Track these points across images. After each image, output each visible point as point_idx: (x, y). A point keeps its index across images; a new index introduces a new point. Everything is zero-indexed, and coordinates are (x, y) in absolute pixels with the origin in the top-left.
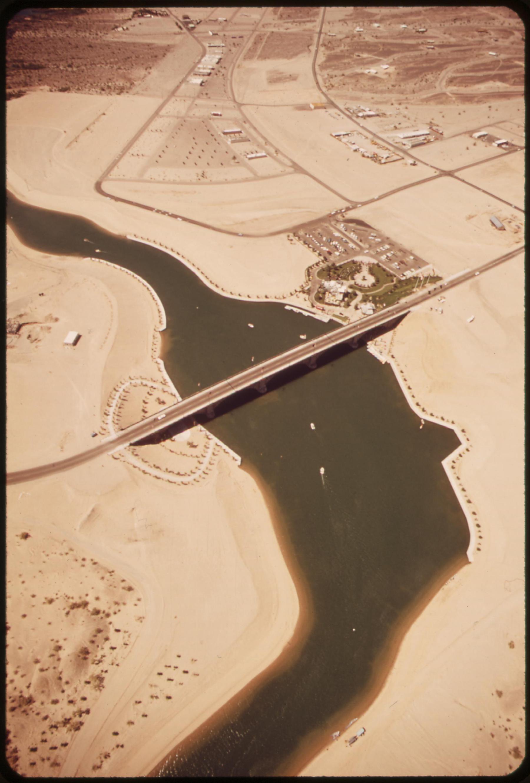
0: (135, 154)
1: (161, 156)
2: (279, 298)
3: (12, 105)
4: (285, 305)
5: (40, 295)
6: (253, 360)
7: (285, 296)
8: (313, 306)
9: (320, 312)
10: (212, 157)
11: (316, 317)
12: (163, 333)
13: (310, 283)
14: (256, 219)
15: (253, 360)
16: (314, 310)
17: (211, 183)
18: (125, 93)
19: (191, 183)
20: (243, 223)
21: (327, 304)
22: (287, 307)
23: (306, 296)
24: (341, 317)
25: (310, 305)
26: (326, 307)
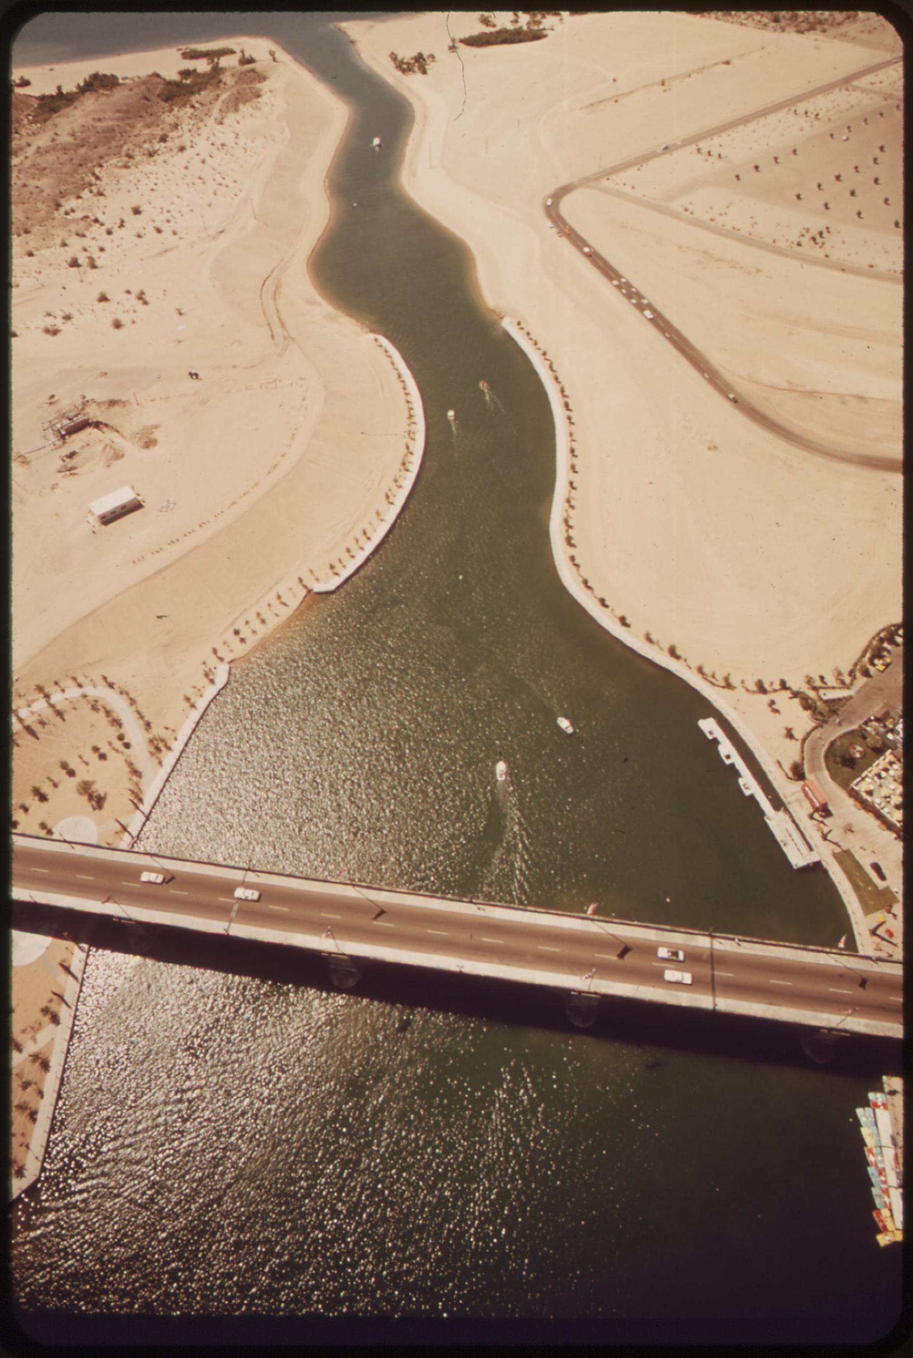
0: (714, 159)
1: (760, 169)
2: (710, 679)
3: (897, 617)
4: (711, 711)
5: (191, 375)
6: (515, 1236)
7: (734, 680)
8: (798, 773)
9: (801, 811)
10: (886, 201)
11: (776, 822)
12: (315, 598)
13: (861, 680)
14: (862, 399)
15: (515, 1236)
16: (787, 789)
17: (826, 262)
18: (818, 32)
19: (773, 248)
20: (812, 394)
21: (854, 795)
22: (708, 726)
23: (803, 721)
24: (869, 882)
25: (791, 752)
26: (844, 805)
